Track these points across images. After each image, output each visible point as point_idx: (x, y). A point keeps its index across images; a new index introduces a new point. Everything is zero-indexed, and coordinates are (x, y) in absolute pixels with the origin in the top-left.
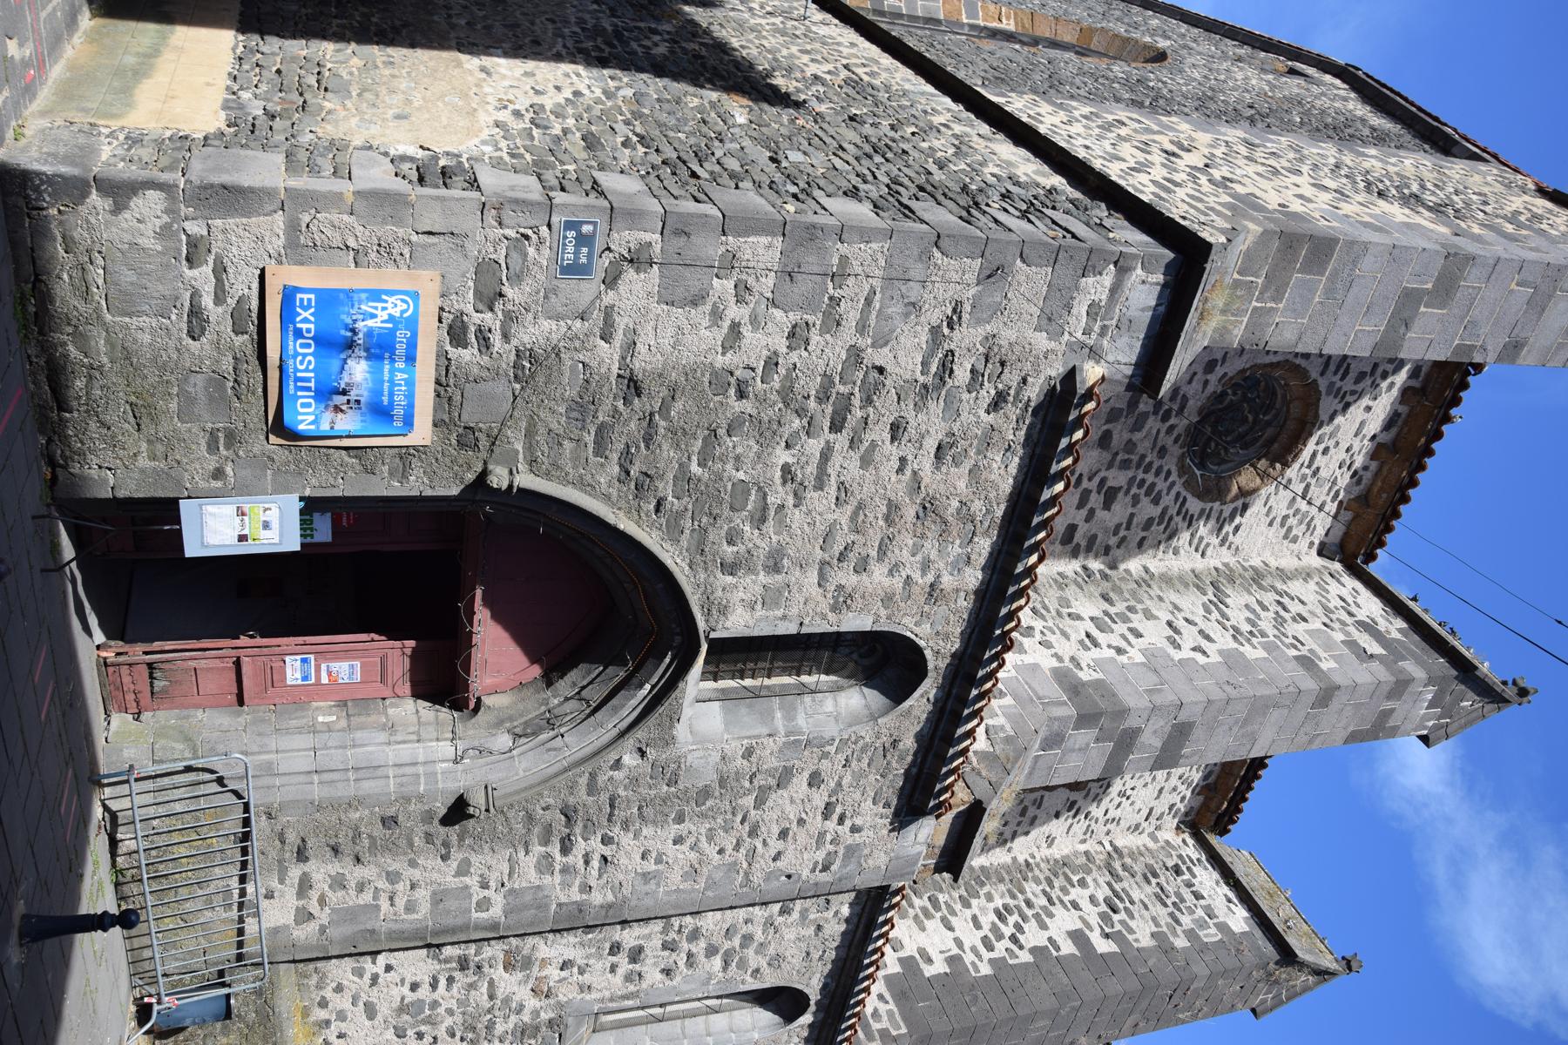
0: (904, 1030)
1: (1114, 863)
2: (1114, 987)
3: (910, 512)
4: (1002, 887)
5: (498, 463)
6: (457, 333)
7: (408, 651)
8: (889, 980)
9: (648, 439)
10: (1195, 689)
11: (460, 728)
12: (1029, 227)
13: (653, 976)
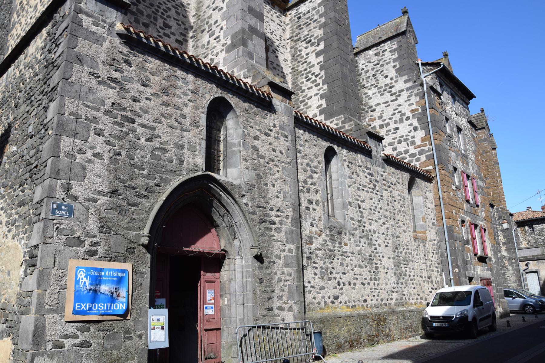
0: (343, 116)
1: (294, 39)
2: (335, 44)
3: (166, 98)
4: (299, 78)
5: (140, 241)
6: (92, 254)
7: (204, 273)
8: (326, 119)
9: (134, 188)
10: (237, 4)
11: (231, 257)
12: (62, 44)
13: (318, 197)
